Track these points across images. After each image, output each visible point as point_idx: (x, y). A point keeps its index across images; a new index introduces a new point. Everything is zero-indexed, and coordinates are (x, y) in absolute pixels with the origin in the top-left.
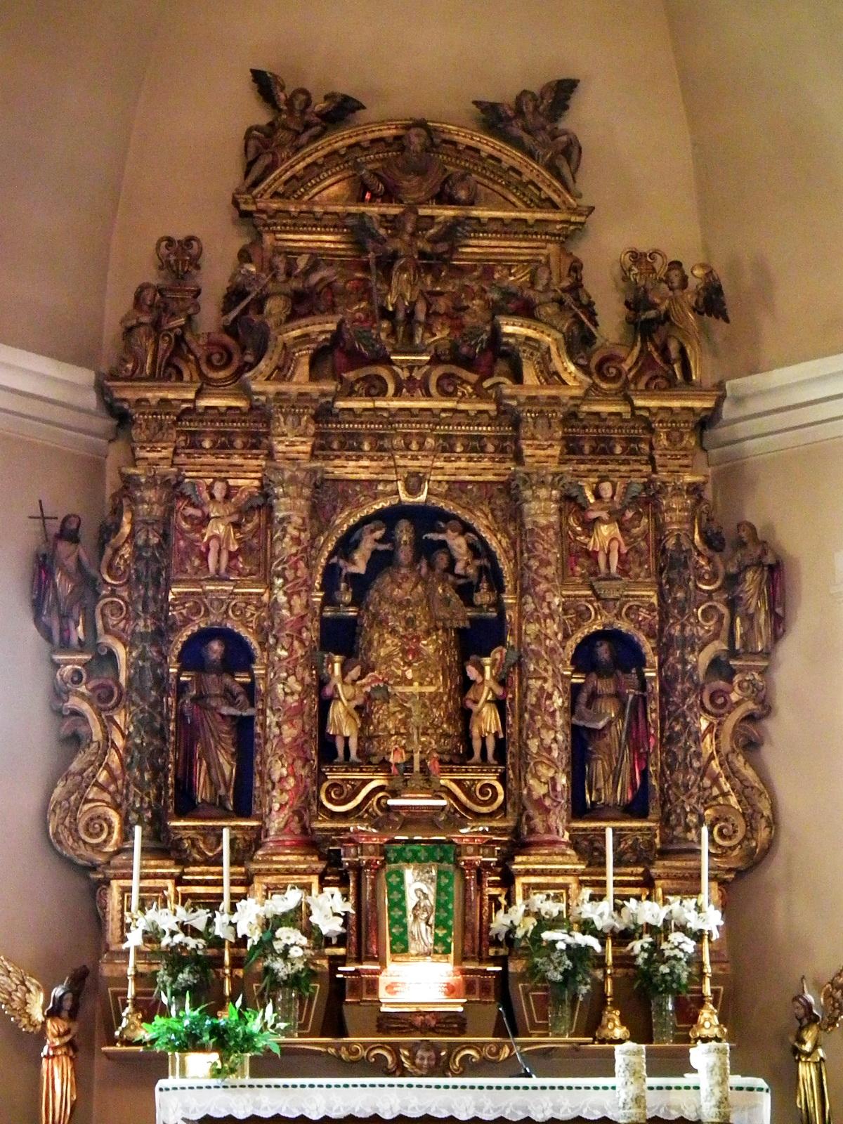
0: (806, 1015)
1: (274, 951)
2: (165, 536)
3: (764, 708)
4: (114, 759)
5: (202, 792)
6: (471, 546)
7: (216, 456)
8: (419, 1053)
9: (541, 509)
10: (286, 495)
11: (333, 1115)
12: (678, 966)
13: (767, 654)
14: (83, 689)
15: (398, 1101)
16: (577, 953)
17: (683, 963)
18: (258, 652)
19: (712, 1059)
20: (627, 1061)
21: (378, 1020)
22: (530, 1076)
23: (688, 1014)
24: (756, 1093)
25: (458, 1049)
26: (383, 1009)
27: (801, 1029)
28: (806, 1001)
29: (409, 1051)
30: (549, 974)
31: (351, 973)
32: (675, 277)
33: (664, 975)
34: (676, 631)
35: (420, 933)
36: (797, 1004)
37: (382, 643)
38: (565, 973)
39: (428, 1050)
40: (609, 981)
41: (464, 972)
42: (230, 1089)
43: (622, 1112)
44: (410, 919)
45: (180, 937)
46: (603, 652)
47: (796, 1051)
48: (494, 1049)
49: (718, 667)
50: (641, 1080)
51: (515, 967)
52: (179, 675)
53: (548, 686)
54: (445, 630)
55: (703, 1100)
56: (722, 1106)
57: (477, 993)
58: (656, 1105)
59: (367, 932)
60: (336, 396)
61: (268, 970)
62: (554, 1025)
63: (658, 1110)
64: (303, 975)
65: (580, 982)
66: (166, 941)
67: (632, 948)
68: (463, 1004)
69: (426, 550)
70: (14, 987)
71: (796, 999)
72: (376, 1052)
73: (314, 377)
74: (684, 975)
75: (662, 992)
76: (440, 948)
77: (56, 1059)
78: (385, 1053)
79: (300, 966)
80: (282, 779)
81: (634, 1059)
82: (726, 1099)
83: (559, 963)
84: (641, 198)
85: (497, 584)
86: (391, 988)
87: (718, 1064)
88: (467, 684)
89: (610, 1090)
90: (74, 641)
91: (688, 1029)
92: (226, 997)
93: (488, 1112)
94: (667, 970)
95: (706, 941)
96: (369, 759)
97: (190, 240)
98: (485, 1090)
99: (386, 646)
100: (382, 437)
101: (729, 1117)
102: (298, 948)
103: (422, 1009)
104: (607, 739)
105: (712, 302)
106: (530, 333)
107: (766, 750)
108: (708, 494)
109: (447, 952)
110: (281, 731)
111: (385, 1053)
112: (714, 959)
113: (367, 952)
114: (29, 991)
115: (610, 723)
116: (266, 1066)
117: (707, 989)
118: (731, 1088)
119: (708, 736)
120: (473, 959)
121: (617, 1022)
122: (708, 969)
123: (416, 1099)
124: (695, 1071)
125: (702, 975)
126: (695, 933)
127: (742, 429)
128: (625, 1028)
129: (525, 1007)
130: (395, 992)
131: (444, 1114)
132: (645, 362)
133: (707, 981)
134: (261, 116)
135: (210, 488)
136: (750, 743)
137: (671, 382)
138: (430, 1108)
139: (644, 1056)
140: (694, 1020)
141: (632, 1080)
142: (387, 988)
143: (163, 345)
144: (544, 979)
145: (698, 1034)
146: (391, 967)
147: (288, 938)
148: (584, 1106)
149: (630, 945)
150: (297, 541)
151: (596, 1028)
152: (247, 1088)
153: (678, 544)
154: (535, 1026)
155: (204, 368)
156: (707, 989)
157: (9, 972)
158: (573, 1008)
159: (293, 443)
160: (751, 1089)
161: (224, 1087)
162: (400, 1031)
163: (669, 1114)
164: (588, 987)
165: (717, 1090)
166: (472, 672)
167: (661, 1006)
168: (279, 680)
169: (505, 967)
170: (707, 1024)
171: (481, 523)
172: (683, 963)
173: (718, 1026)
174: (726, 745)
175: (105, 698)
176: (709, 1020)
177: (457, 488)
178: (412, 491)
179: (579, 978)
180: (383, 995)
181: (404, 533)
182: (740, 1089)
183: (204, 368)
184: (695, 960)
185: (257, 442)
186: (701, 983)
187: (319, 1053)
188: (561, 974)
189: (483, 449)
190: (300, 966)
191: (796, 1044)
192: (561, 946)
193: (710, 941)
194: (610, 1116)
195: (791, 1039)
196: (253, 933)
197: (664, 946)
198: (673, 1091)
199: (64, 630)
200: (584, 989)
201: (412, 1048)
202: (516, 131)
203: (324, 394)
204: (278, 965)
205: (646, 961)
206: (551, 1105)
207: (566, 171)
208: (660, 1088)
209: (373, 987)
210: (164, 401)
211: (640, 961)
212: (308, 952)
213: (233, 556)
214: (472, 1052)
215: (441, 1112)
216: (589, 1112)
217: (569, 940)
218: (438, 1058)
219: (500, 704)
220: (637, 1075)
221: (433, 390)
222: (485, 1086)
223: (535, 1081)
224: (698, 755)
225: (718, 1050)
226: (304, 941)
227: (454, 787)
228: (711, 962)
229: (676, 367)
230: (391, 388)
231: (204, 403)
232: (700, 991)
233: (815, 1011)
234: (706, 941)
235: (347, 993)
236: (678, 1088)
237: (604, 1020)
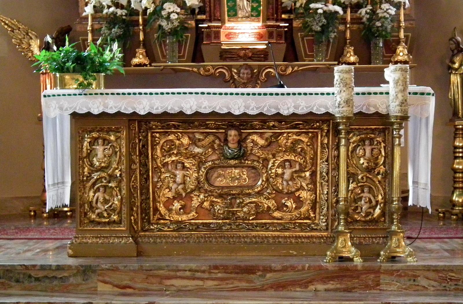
0: (456, 48)
1: (162, 17)
8: (242, 71)
11: (154, 112)
12: (386, 22)
15: (195, 103)
16: (330, 16)
17: (389, 20)
19: (397, 75)
20: (341, 78)
21: (221, 53)
22: (284, 87)
23: (391, 49)
24: (425, 96)
25: (264, 68)
26: (223, 47)
27: (453, 56)
28: (456, 40)
29: (237, 70)
30: (313, 27)
31: (206, 28)
33: (378, 27)
35: (243, 5)
36: (451, 42)
38: (322, 26)
39: (246, 69)
40: (348, 31)
41: (268, 27)
42: (89, 96)
43: (337, 109)
45: (112, 9)
47: (450, 68)
48: (283, 68)
50: (350, 89)
51: (296, 24)
55: (391, 102)
56: (403, 105)
57: (275, 37)
58: (360, 104)
59: (214, 6)
61: (160, 26)
62: (317, 55)
63: (263, 109)
64: (179, 29)
65: (331, 31)
66: (105, 11)
67: (361, 13)
68: (266, 44)
70: (23, 36)
71: (451, 39)
72: (219, 70)
74: (389, 27)
75: (377, 37)
76: (255, 14)
77: (47, 75)
78: (224, 71)
79: (176, 24)
81: (346, 76)
82: (406, 100)
83: (319, 21)
86: (228, 36)
87: (402, 78)
89: (331, 95)
91: (391, 57)
92: (140, 41)
93: (253, 109)
94: (380, 25)
95: (402, 8)
98: (251, 96)
101: (407, 112)
102: (175, 14)
103: (245, 47)
109: (258, 15)
111: (224, 71)
112: (407, 19)
113: (215, 16)
114: (31, 38)
116: (114, 81)
117: (402, 35)
118: (410, 93)
120: (273, 19)
121: (352, 54)
122: (403, 24)
123: (207, 102)
124: (388, 83)
125: (399, 27)
126: (396, 3)
128: (356, 57)
129: (301, 46)
130: (230, 38)
131: (225, 111)
133: (402, 30)
138: (215, 108)
139: (353, 74)
140: (394, 52)
141: (345, 89)
142: (226, 36)
144: (311, 30)
145: (396, 59)
146: (228, 24)
147: (170, 8)
148: (314, 105)
149: (359, 12)
151: (340, 57)
152: (99, 95)
154: (307, 56)
156: (402, 35)
157: (20, 28)
158: (328, 46)
160: (422, 94)
161: (85, 94)
162: (232, 59)
163: (368, 109)
164: (335, 34)
165: (400, 95)
167: (376, 44)
170: (401, 54)
172: (389, 20)
173: (407, 55)
176: (402, 52)
179: (330, 29)
180: (223, 38)
182: (416, 93)
184: (396, 19)
186: (399, 32)
187: (188, 71)
188: (321, 27)
190: (176, 24)
191: (450, 64)
192: (320, 11)
193: (404, 9)
194: (331, 111)
195: (447, 61)
196: (151, 6)
197: (379, 11)
198: (372, 95)
200: (333, 35)
201: (239, 68)
204: (164, 23)
205: (369, 20)
206: (293, 105)
208: (363, 94)
209: (217, 35)
211: (365, 19)
212: (181, 16)
214: (271, 70)
215: (223, 110)
216: (268, 110)
217: (325, 8)
218: (252, 73)
220: (348, 86)
222: (251, 93)
223: (286, 90)
225: (401, 70)
226: (179, 10)
228: (405, 20)
232: (398, 36)
233: (461, 46)
234: (402, 8)
235: (204, 39)
236: (375, 93)
237: (345, 53)
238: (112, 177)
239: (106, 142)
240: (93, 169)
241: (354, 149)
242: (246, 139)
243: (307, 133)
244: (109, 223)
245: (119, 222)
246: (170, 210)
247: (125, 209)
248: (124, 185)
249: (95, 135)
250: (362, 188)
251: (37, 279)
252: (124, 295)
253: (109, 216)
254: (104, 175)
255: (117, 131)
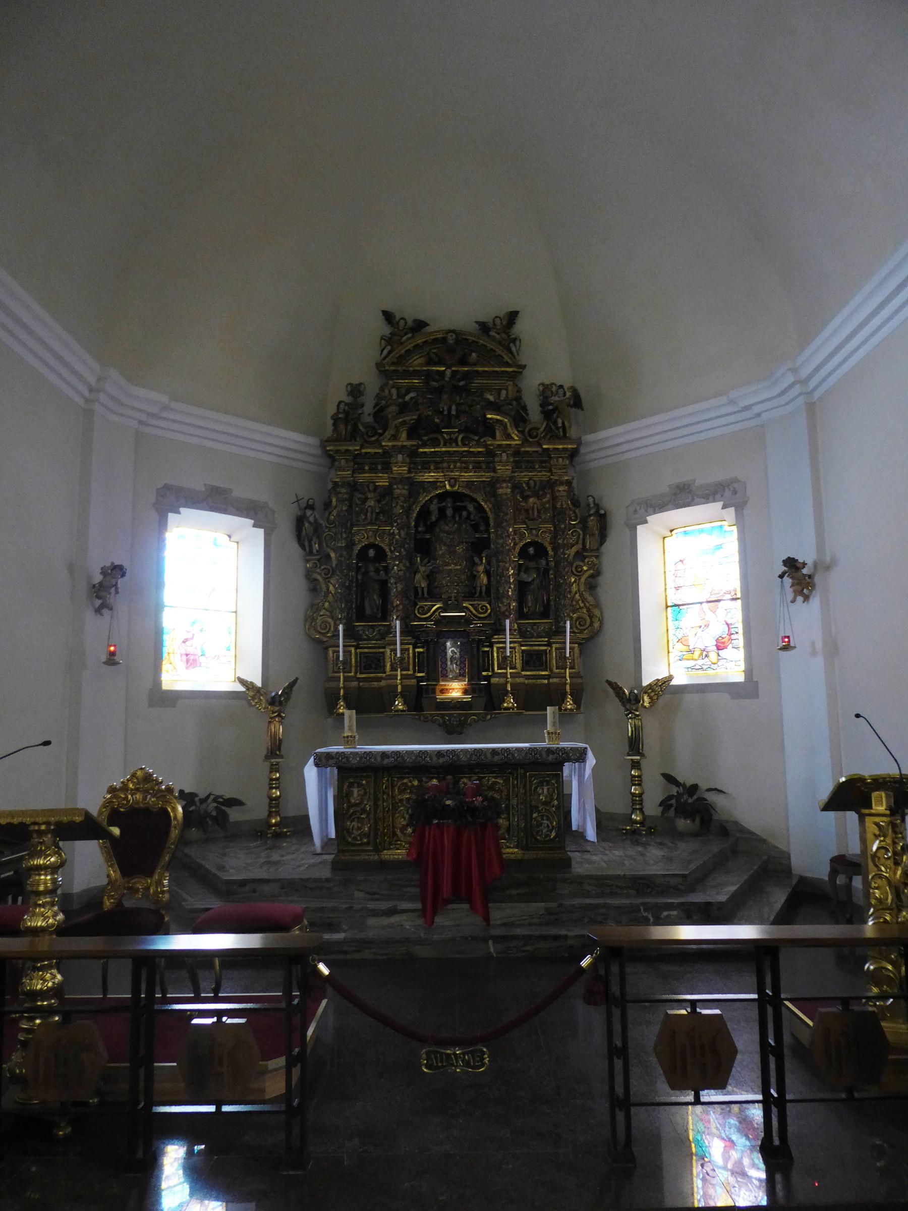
2: (350, 507)
3: (597, 573)
4: (330, 598)
5: (368, 611)
6: (475, 507)
7: (370, 473)
9: (505, 490)
10: (398, 488)
13: (598, 550)
14: (318, 570)
18: (389, 553)
32: (561, 391)
34: (560, 541)
37: (441, 549)
44: (449, 663)
46: (531, 550)
49: (580, 556)
52: (357, 563)
53: (507, 565)
54: (466, 543)
60: (419, 446)
69: (458, 510)
73: (410, 437)
80: (397, 606)
84: (546, 362)
85: (488, 525)
88: (474, 564)
90: (315, 551)
96: (433, 595)
97: (360, 384)
99: (441, 550)
100: (438, 463)
104: (533, 586)
105: (577, 401)
106: (498, 417)
107: (598, 589)
108: (575, 484)
110: (395, 588)
115: (533, 580)
119: (575, 584)
127: (587, 458)
132: (548, 430)
134: (386, 330)
135: (368, 486)
136: (592, 587)
137: (558, 437)
143: (349, 427)
150: (402, 507)
153: (562, 505)
155: (365, 436)
159: (400, 469)
162: (445, 709)
166: (476, 560)
168: (395, 565)
169: (489, 681)
171: (480, 498)
174: (582, 589)
175: (329, 574)
177: (469, 484)
178: (452, 486)
181: (449, 503)
183: (365, 436)
185: (387, 467)
189: (480, 467)
199: (311, 546)
202: (492, 333)
203: (413, 446)
207: (514, 349)
210: (347, 450)
213: (378, 514)
219: (487, 573)
221: (460, 443)
224: (570, 592)
227: (470, 607)
229: (561, 430)
230: (442, 442)
231: (364, 451)
238: (364, 811)
239: (360, 785)
240: (351, 806)
241: (536, 788)
242: (459, 781)
243: (502, 777)
244: (361, 845)
245: (368, 844)
246: (405, 834)
247: (372, 834)
248: (372, 816)
249: (351, 780)
250: (542, 816)
251: (311, 889)
252: (372, 899)
253: (361, 839)
254: (358, 809)
255: (366, 777)
